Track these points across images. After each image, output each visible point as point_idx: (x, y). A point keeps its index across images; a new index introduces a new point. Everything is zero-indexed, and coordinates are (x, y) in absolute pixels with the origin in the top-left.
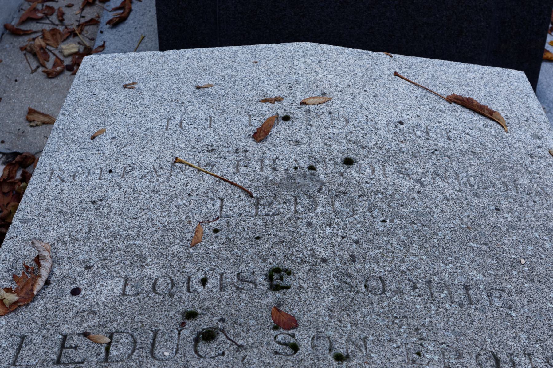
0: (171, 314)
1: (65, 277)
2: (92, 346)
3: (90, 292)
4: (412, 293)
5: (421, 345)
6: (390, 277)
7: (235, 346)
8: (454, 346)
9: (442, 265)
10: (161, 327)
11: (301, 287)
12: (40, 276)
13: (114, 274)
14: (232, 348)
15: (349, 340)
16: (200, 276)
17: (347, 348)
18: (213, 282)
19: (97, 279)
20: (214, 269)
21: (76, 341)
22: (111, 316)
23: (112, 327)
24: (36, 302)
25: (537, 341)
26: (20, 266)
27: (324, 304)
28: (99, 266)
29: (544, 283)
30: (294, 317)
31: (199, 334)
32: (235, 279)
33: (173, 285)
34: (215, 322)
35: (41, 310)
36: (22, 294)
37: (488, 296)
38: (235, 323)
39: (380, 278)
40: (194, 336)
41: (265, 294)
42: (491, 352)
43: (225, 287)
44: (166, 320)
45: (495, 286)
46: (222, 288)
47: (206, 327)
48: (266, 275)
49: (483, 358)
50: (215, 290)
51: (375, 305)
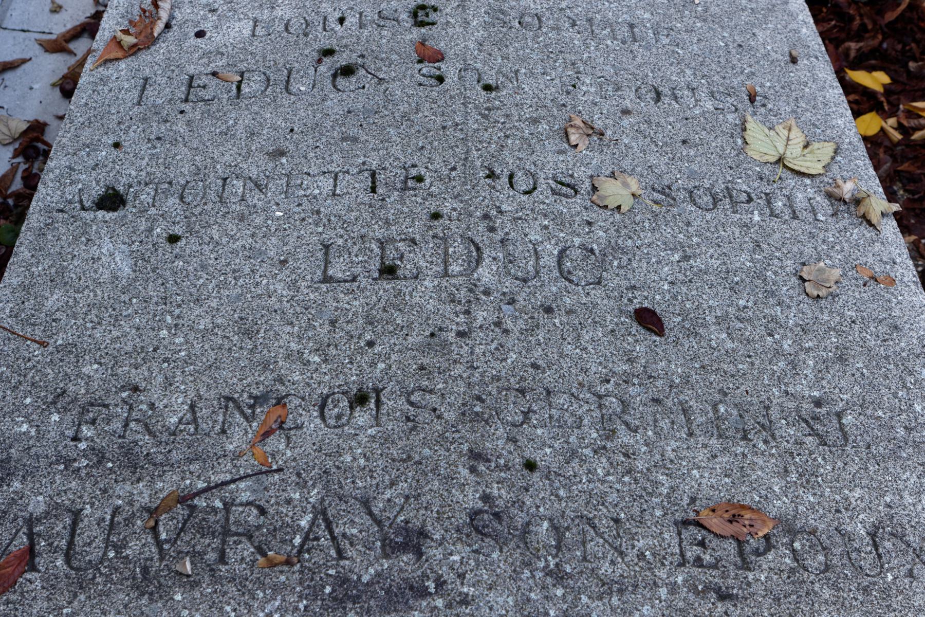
0: (307, 52)
1: (187, 20)
2: (222, 84)
3: (216, 34)
4: (571, 30)
5: (578, 78)
6: (547, 14)
7: (376, 80)
8: (613, 80)
9: (606, 3)
10: (296, 65)
11: (448, 22)
12: (159, 18)
13: (242, 16)
14: (373, 81)
15: (499, 72)
16: (338, 15)
17: (497, 80)
18: (352, 20)
19: (223, 22)
20: (353, 8)
21: (204, 80)
22: (241, 56)
23: (243, 66)
24: (158, 46)
25: (703, 77)
26: (136, 11)
27: (473, 39)
28: (224, 8)
29: (717, 23)
30: (440, 51)
31: (337, 70)
32: (376, 17)
33: (307, 25)
34: (354, 58)
35: (164, 53)
36: (142, 38)
37: (654, 34)
38: (376, 58)
39: (536, 15)
40: (332, 72)
41: (409, 30)
42: (653, 86)
43: (365, 25)
44: (300, 58)
45: (662, 25)
46: (362, 26)
47: (344, 63)
48: (410, 12)
49: (643, 91)
50: (353, 28)
51: (529, 40)
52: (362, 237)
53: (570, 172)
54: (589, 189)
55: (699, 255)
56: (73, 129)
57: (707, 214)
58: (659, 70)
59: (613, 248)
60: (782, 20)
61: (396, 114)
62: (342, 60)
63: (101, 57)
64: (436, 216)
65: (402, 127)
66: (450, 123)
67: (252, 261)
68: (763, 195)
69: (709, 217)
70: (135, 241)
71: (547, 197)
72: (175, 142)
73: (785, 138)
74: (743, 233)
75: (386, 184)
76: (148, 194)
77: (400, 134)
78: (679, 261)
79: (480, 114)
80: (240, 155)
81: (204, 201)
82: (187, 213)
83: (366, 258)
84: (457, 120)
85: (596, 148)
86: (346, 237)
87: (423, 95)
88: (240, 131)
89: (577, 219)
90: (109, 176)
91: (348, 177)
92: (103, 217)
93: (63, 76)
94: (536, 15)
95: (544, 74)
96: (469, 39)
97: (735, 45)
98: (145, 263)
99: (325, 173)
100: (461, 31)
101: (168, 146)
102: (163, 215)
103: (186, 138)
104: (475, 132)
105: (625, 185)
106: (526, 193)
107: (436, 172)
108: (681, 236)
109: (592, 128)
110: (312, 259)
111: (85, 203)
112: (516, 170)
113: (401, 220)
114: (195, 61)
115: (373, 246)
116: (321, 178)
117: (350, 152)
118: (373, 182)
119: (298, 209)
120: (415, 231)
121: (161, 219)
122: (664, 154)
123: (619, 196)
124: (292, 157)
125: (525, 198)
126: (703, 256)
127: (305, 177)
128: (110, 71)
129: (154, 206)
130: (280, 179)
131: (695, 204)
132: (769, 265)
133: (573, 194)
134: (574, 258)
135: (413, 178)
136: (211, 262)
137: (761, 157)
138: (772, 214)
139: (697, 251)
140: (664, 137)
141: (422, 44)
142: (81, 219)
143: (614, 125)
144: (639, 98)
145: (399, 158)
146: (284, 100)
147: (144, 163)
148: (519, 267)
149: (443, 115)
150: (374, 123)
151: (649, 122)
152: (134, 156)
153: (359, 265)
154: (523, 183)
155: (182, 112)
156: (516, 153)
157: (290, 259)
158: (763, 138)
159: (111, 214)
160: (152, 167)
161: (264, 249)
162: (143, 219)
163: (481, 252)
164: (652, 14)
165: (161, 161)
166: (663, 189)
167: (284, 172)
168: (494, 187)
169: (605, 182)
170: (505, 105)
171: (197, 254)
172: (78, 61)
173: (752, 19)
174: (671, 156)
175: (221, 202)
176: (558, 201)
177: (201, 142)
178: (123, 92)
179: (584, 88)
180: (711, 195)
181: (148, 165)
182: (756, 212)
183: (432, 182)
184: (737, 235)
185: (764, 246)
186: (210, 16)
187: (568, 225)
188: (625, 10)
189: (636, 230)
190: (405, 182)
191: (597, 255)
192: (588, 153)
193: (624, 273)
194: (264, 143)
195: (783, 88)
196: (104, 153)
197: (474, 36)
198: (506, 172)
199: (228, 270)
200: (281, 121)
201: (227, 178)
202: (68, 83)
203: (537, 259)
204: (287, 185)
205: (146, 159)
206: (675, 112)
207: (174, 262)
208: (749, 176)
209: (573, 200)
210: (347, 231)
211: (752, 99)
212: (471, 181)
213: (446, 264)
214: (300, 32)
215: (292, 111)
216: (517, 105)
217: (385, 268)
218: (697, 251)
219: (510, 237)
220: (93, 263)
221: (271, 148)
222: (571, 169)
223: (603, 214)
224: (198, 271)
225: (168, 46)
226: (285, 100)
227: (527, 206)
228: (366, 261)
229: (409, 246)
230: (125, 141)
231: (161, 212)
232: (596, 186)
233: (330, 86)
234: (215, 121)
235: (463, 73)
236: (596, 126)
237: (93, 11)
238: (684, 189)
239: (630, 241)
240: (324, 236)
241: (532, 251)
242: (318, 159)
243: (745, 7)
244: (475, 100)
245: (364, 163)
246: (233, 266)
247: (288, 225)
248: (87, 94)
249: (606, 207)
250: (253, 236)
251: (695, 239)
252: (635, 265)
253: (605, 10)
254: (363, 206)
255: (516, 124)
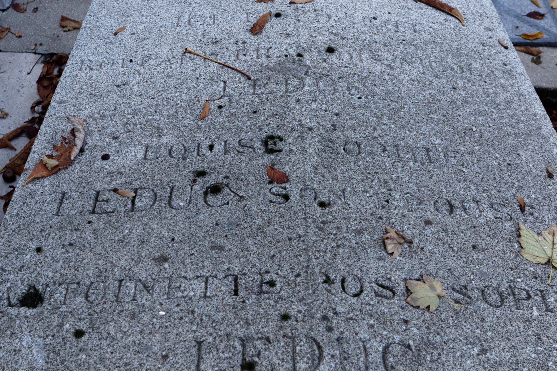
0: (185, 173)
1: (96, 146)
2: (121, 199)
3: (117, 158)
4: (383, 155)
5: (390, 194)
6: (365, 142)
7: (237, 197)
8: (416, 195)
9: (408, 132)
10: (177, 184)
11: (291, 150)
12: (75, 145)
13: (137, 143)
14: (235, 199)
15: (330, 191)
16: (208, 143)
17: (329, 197)
18: (219, 147)
19: (123, 147)
20: (219, 138)
21: (107, 195)
22: (135, 175)
23: (136, 184)
24: (74, 166)
25: (484, 191)
26: (59, 138)
27: (310, 163)
29: (491, 146)
30: (285, 173)
32: (237, 145)
33: (186, 151)
35: (78, 172)
36: (62, 160)
37: (445, 156)
38: (237, 179)
39: (356, 143)
40: (204, 190)
42: (447, 199)
43: (229, 151)
44: (180, 178)
45: (450, 149)
46: (226, 152)
47: (213, 183)
48: (262, 141)
49: (440, 204)
51: (352, 164)
52: (228, 335)
53: (389, 276)
54: (404, 290)
55: (494, 348)
56: (6, 235)
57: (497, 311)
58: (450, 186)
59: (425, 344)
60: (538, 143)
61: (253, 227)
62: (211, 180)
63: (31, 176)
64: (285, 317)
65: (258, 238)
66: (294, 235)
67: (140, 355)
68: (538, 292)
69: (499, 313)
70: (49, 335)
71: (372, 299)
72: (83, 248)
73: (551, 242)
74: (526, 327)
75: (246, 288)
76: (61, 293)
77: (256, 244)
78: (478, 355)
79: (317, 227)
80: (133, 260)
81: (104, 300)
82: (91, 311)
83: (231, 355)
84: (300, 233)
85: (407, 254)
86: (215, 335)
87: (273, 211)
88: (134, 240)
89: (396, 318)
90: (31, 277)
91: (216, 281)
92: (25, 313)
93: (6, 167)
94: (356, 143)
95: (364, 192)
96: (307, 164)
97: (506, 164)
98: (56, 355)
99: (198, 277)
100: (301, 157)
101: (78, 251)
102: (71, 312)
103: (92, 244)
104: (314, 243)
105: (432, 288)
106: (355, 295)
107: (284, 278)
108: (478, 331)
109: (404, 238)
110: (187, 355)
111: (11, 300)
112: (346, 275)
113: (258, 321)
114: (101, 179)
115: (237, 344)
116: (196, 281)
117: (218, 259)
118: (236, 286)
119: (177, 309)
120: (269, 330)
121: (70, 316)
122: (459, 258)
123: (428, 298)
124: (173, 263)
125: (354, 300)
126: (497, 349)
127: (183, 280)
128: (37, 187)
129: (65, 304)
130: (164, 282)
131: (486, 302)
132: (550, 356)
133: (392, 295)
134: (395, 354)
135: (267, 283)
136: (108, 356)
137: (534, 259)
138: (548, 310)
139: (491, 344)
140: (458, 243)
141: (272, 168)
142: (8, 314)
143: (420, 234)
144: (437, 210)
145: (255, 265)
146: (167, 213)
147: (59, 265)
148: (352, 363)
149: (289, 228)
150: (236, 234)
151: (446, 231)
152: (51, 260)
153: (225, 361)
154: (352, 287)
155: (90, 222)
156: (346, 260)
157: (170, 355)
158: (535, 244)
159: (31, 311)
160: (65, 269)
161: (150, 344)
162: (56, 316)
163: (322, 350)
164: (442, 140)
165: (72, 264)
166: (461, 289)
167: (166, 275)
168: (330, 291)
169: (416, 285)
170: (336, 219)
171: (97, 348)
172: (17, 155)
173: (516, 142)
174: (465, 260)
175: (117, 301)
176: (381, 302)
177: (103, 248)
178: (46, 204)
179: (395, 203)
180: (498, 294)
181: (62, 267)
182: (535, 308)
183: (282, 287)
184: (522, 329)
185: (544, 339)
186: (113, 142)
187: (389, 324)
188: (422, 137)
189: (442, 327)
190: (261, 286)
191: (414, 350)
192: (401, 259)
193: (436, 367)
194: (151, 250)
195: (544, 199)
196: (28, 256)
197: (310, 161)
198: (339, 278)
199: (121, 364)
200: (165, 231)
201: (122, 280)
202: (9, 172)
203: (367, 355)
204: (169, 287)
205: (61, 262)
206: (465, 221)
207: (79, 355)
208: (526, 276)
209: (392, 301)
210: (216, 330)
211: (522, 209)
212: (312, 286)
213: (294, 361)
214: (180, 156)
215: (174, 223)
216: (345, 219)
217: (246, 364)
218: (491, 344)
219: (345, 336)
220: (15, 355)
221: (157, 255)
222: (389, 273)
223: (416, 313)
224: (97, 364)
225: (81, 167)
226: (168, 213)
227: (356, 307)
228: (230, 358)
229: (265, 345)
230: (45, 246)
231: (70, 310)
232: (410, 288)
233: (203, 202)
234: (114, 231)
235: (303, 192)
236: (406, 236)
237: (30, 118)
238: (477, 288)
239: (438, 337)
240: (197, 333)
241: (362, 348)
242: (193, 265)
243: (510, 132)
244: (313, 215)
245: (228, 269)
246: (125, 360)
247: (169, 323)
248: (19, 205)
249: (418, 307)
250: (141, 332)
251: (489, 334)
252: (444, 359)
253: (407, 137)
254: (228, 308)
255: (345, 235)
